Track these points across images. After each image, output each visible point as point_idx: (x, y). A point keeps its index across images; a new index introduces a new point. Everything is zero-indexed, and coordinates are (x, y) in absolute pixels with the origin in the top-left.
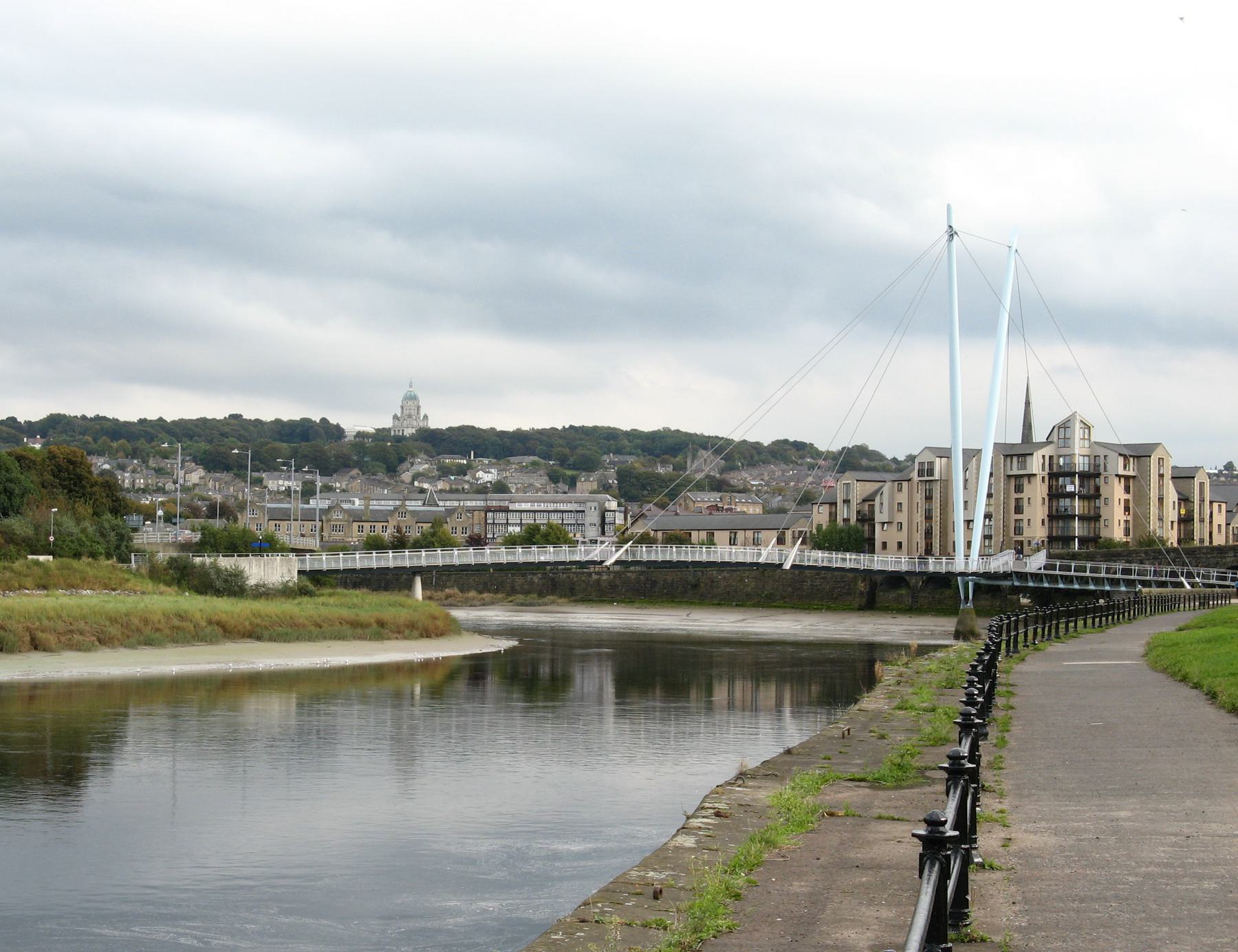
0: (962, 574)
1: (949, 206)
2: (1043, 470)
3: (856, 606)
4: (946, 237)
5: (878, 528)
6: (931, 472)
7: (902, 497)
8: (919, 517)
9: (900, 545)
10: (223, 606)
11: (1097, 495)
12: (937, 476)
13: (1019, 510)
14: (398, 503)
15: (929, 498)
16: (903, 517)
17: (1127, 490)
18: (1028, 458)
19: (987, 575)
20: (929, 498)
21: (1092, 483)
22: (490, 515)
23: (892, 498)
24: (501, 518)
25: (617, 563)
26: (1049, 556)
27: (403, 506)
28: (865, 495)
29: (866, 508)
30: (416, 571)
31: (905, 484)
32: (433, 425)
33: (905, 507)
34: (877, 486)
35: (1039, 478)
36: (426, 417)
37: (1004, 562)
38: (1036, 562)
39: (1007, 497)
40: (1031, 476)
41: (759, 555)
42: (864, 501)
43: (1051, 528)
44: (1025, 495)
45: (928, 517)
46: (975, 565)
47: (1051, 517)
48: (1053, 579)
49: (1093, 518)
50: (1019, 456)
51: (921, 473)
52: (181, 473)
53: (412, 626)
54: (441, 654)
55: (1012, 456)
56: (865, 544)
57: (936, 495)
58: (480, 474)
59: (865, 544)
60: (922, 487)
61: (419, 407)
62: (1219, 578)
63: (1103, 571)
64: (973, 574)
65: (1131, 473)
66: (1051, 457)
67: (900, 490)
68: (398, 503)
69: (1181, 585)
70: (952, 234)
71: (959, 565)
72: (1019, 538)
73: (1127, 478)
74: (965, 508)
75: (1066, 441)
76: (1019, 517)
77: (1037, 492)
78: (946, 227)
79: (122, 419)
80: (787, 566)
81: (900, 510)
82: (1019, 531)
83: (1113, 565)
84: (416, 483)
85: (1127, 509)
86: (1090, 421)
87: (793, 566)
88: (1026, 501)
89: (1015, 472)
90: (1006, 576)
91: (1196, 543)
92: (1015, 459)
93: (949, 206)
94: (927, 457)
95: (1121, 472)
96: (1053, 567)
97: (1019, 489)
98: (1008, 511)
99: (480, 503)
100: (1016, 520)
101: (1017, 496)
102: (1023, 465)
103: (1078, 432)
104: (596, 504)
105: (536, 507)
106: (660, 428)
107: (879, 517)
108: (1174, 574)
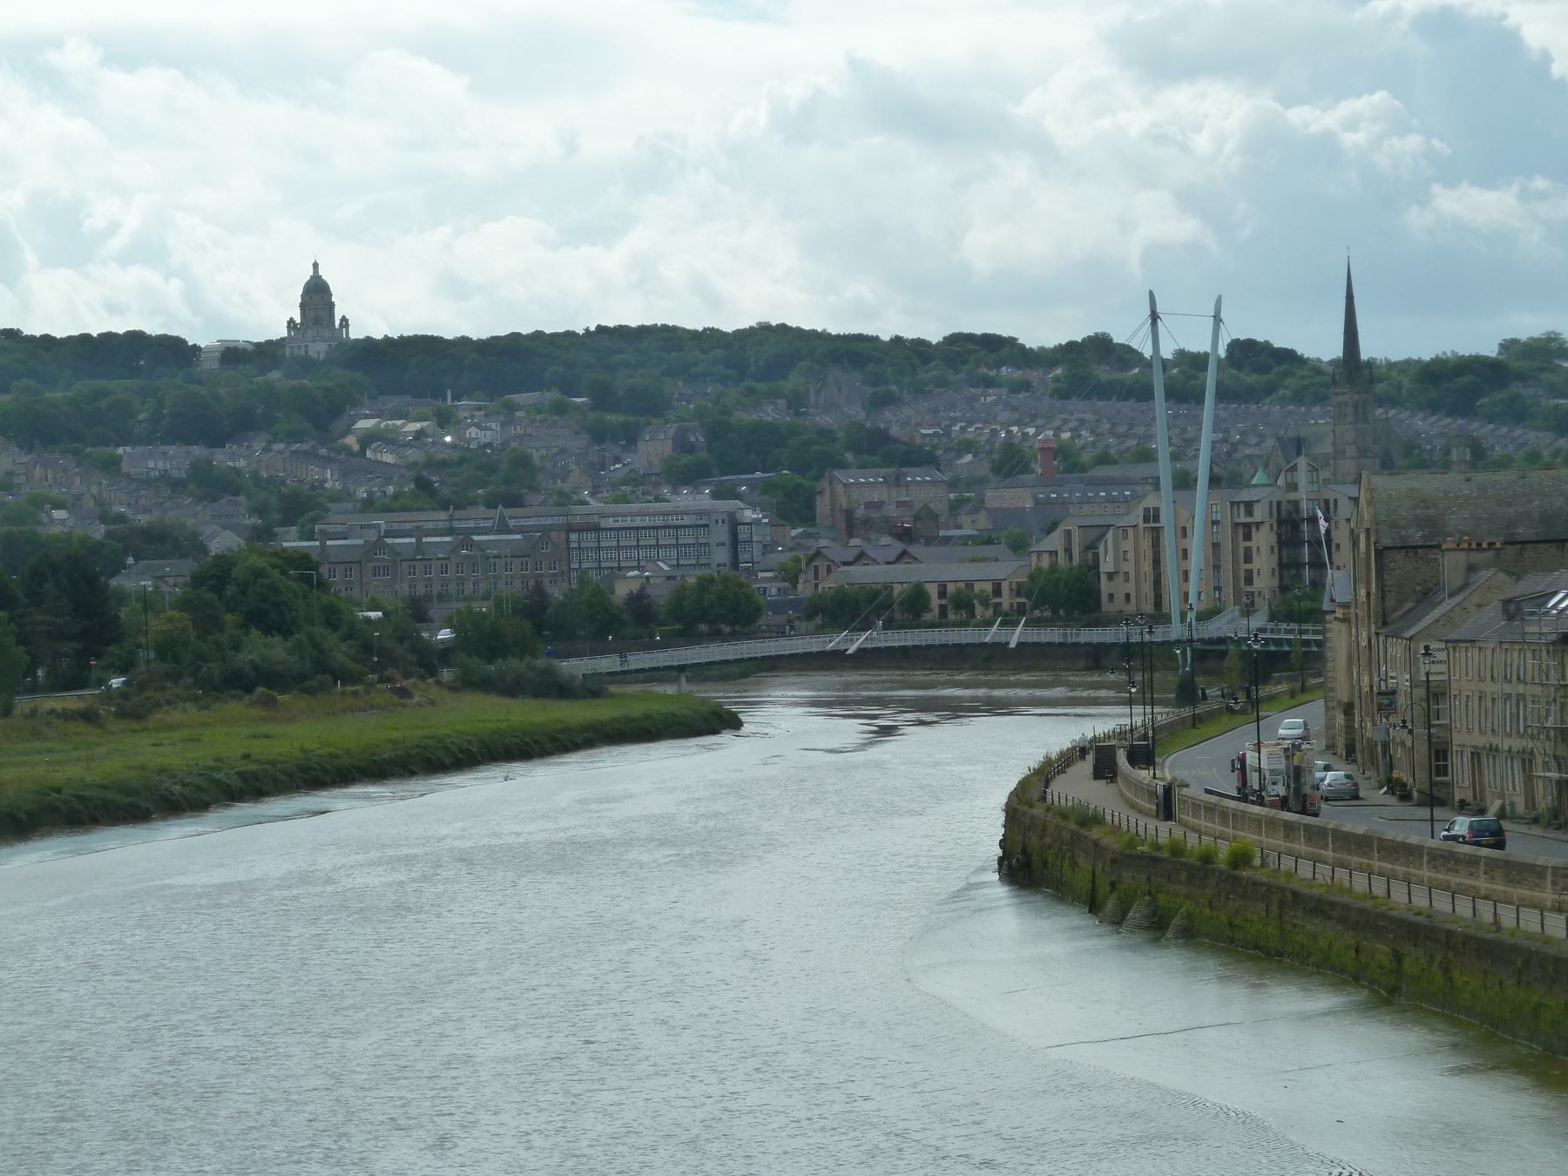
1: (1151, 294)
3: (1216, 470)
5: (1103, 578)
6: (1157, 519)
7: (1128, 545)
9: (1128, 596)
13: (1248, 558)
16: (1129, 567)
22: (574, 536)
23: (1116, 547)
24: (589, 539)
29: (1090, 556)
31: (1130, 531)
32: (356, 333)
33: (1131, 556)
34: (1101, 530)
36: (344, 320)
43: (1281, 578)
51: (1146, 520)
61: (331, 306)
66: (1279, 503)
70: (1154, 317)
74: (1186, 573)
77: (1264, 540)
80: (1013, 645)
84: (369, 454)
87: (1019, 644)
89: (1243, 519)
92: (1242, 507)
93: (1151, 294)
97: (1248, 537)
99: (562, 520)
102: (1250, 513)
104: (725, 516)
105: (638, 522)
106: (753, 324)
107: (1107, 565)
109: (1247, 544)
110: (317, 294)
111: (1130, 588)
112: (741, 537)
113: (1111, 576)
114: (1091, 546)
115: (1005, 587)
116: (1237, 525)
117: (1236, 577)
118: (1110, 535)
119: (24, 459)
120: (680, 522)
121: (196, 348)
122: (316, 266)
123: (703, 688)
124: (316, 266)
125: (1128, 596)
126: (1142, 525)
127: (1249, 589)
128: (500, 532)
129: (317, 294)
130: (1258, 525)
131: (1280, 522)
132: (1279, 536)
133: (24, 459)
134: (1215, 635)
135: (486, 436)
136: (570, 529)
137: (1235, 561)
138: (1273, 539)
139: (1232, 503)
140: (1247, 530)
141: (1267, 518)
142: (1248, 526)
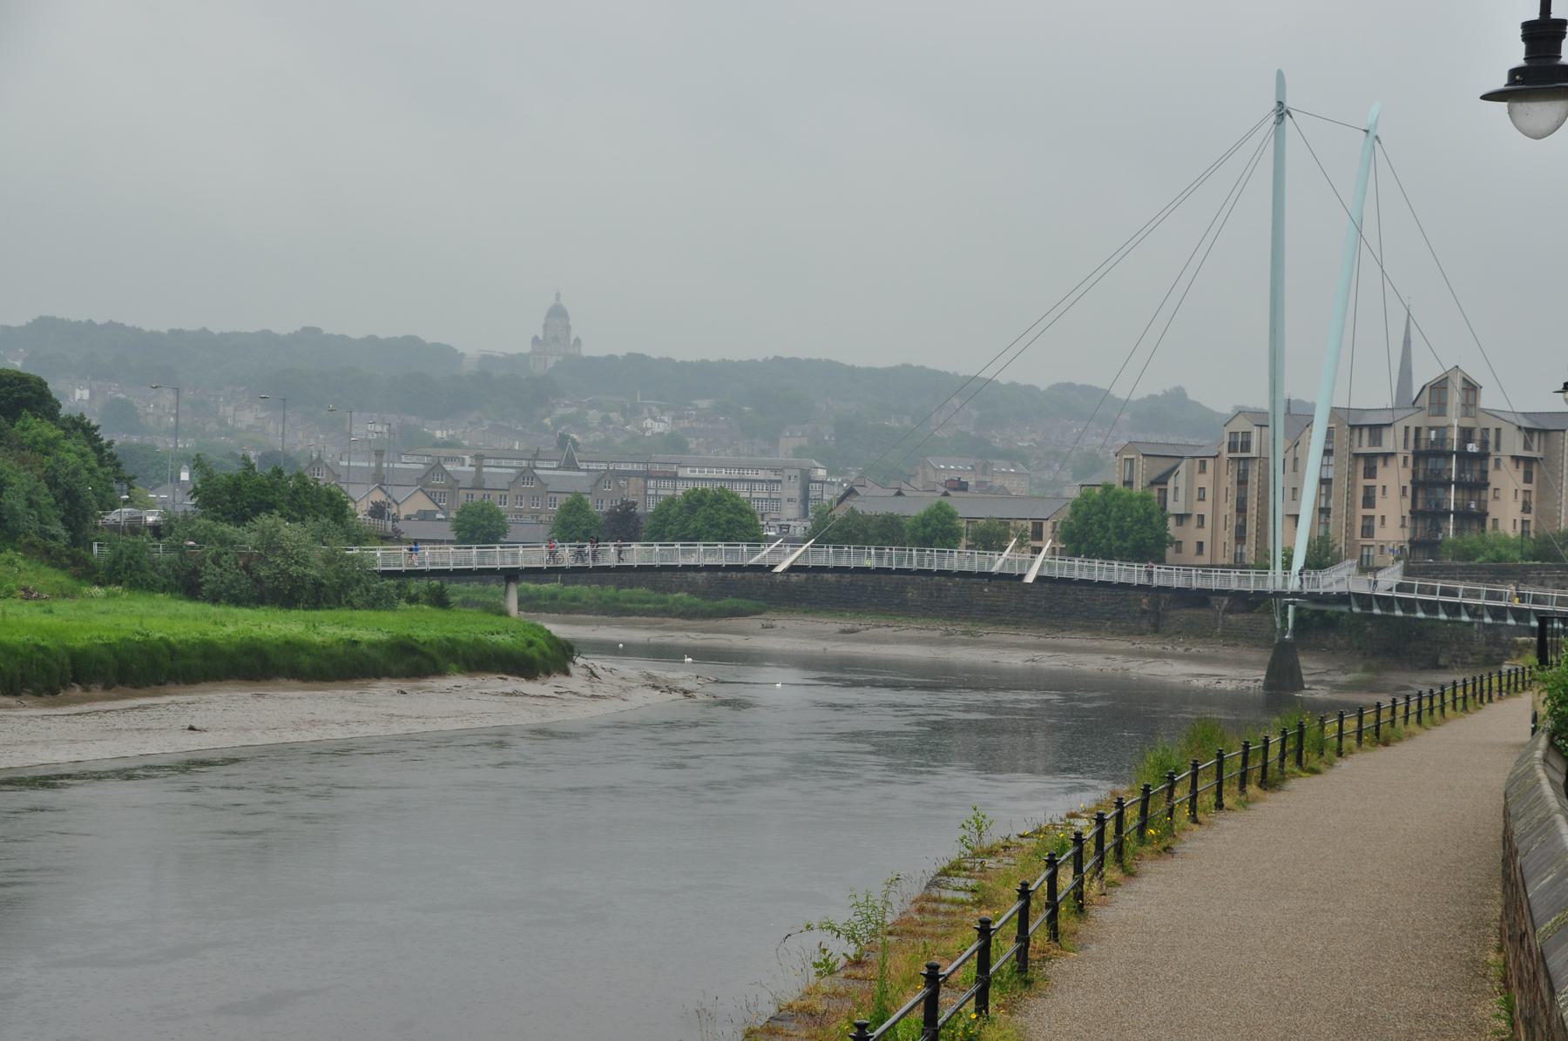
0: (1277, 594)
1: (1280, 75)
2: (1406, 446)
4: (1274, 118)
5: (1171, 522)
6: (1246, 446)
7: (1205, 481)
8: (1228, 508)
9: (1200, 545)
11: (1483, 484)
12: (1254, 453)
13: (1369, 501)
14: (524, 463)
15: (1242, 482)
16: (1205, 508)
17: (1528, 479)
18: (1385, 432)
19: (1314, 597)
20: (1242, 482)
21: (1477, 467)
22: (651, 483)
23: (1190, 480)
25: (793, 569)
26: (1408, 572)
27: (532, 468)
28: (1154, 475)
29: (1155, 493)
31: (1210, 463)
32: (588, 350)
34: (1171, 463)
35: (1400, 459)
36: (578, 341)
37: (1341, 579)
38: (1389, 579)
39: (1352, 484)
41: (992, 562)
42: (1153, 483)
43: (1414, 530)
45: (1241, 509)
48: (1409, 605)
49: (1474, 518)
50: (1372, 427)
51: (1232, 447)
52: (230, 410)
54: (789, 647)
55: (1361, 427)
57: (1253, 478)
58: (649, 422)
59: (1151, 548)
60: (1233, 468)
61: (568, 328)
64: (1294, 594)
66: (1418, 430)
67: (1203, 470)
68: (524, 463)
70: (1282, 112)
71: (1274, 581)
73: (1529, 461)
75: (1440, 407)
77: (1394, 479)
78: (1274, 105)
79: (147, 328)
80: (1029, 579)
81: (1202, 499)
83: (1500, 589)
85: (1526, 508)
86: (1476, 378)
87: (1039, 579)
89: (1366, 449)
90: (1344, 598)
92: (1366, 432)
93: (1280, 75)
94: (1241, 425)
95: (1520, 452)
96: (1410, 589)
97: (1370, 473)
98: (1354, 503)
100: (1365, 517)
101: (1369, 482)
102: (1376, 438)
103: (1455, 398)
104: (797, 472)
107: (1174, 507)
109: (1369, 482)
110: (557, 313)
111: (1205, 535)
112: (812, 494)
113: (1181, 518)
114: (1161, 481)
115: (1047, 528)
116: (1357, 456)
117: (1350, 525)
118: (1182, 468)
119: (263, 415)
120: (754, 477)
121: (463, 355)
122: (558, 296)
123: (1200, 683)
124: (558, 296)
125: (1200, 545)
126: (1226, 455)
127: (1368, 542)
128: (568, 469)
129: (557, 313)
130: (1387, 456)
131: (1417, 455)
132: (1414, 473)
133: (263, 415)
134: (1335, 589)
135: (659, 427)
136: (648, 476)
137: (1351, 503)
138: (1406, 477)
139: (1352, 427)
140: (1370, 463)
141: (1400, 449)
142: (1370, 458)
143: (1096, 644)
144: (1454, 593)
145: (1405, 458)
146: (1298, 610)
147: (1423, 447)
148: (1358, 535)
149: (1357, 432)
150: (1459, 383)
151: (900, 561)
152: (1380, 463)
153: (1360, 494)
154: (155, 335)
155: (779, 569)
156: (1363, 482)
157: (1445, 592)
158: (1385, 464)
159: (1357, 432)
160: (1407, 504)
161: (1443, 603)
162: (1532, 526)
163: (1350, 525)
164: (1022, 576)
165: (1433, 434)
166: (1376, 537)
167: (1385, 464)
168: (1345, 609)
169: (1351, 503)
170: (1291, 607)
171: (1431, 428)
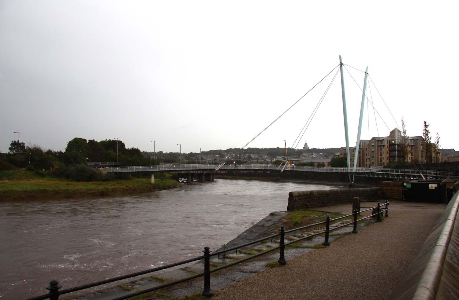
0: (350, 173)
2: (387, 144)
4: (340, 66)
10: (91, 186)
13: (381, 155)
18: (383, 141)
19: (358, 173)
25: (220, 170)
30: (153, 172)
35: (386, 146)
40: (384, 146)
44: (383, 151)
46: (354, 169)
47: (390, 157)
53: (135, 190)
56: (345, 165)
61: (307, 145)
62: (434, 174)
63: (361, 170)
64: (354, 173)
65: (412, 144)
66: (390, 140)
69: (420, 176)
70: (341, 64)
71: (349, 170)
72: (381, 163)
73: (412, 146)
76: (381, 157)
78: (339, 63)
80: (282, 171)
82: (381, 161)
87: (284, 171)
88: (383, 153)
91: (433, 162)
97: (381, 149)
100: (381, 158)
108: (418, 173)
110: (306, 144)
117: (378, 159)
127: (381, 163)
129: (306, 144)
131: (390, 145)
137: (378, 156)
139: (377, 141)
143: (3, 205)
144: (408, 172)
145: (387, 146)
146: (355, 176)
147: (391, 144)
148: (379, 162)
149: (378, 141)
150: (397, 131)
151: (345, 171)
152: (382, 147)
153: (379, 153)
154: (260, 149)
155: (216, 170)
156: (380, 151)
157: (412, 172)
158: (384, 147)
159: (378, 141)
160: (388, 155)
161: (396, 174)
162: (413, 159)
163: (378, 159)
164: (281, 170)
165: (393, 142)
166: (383, 162)
167: (384, 147)
168: (364, 176)
169: (378, 156)
170: (353, 176)
171: (393, 140)
